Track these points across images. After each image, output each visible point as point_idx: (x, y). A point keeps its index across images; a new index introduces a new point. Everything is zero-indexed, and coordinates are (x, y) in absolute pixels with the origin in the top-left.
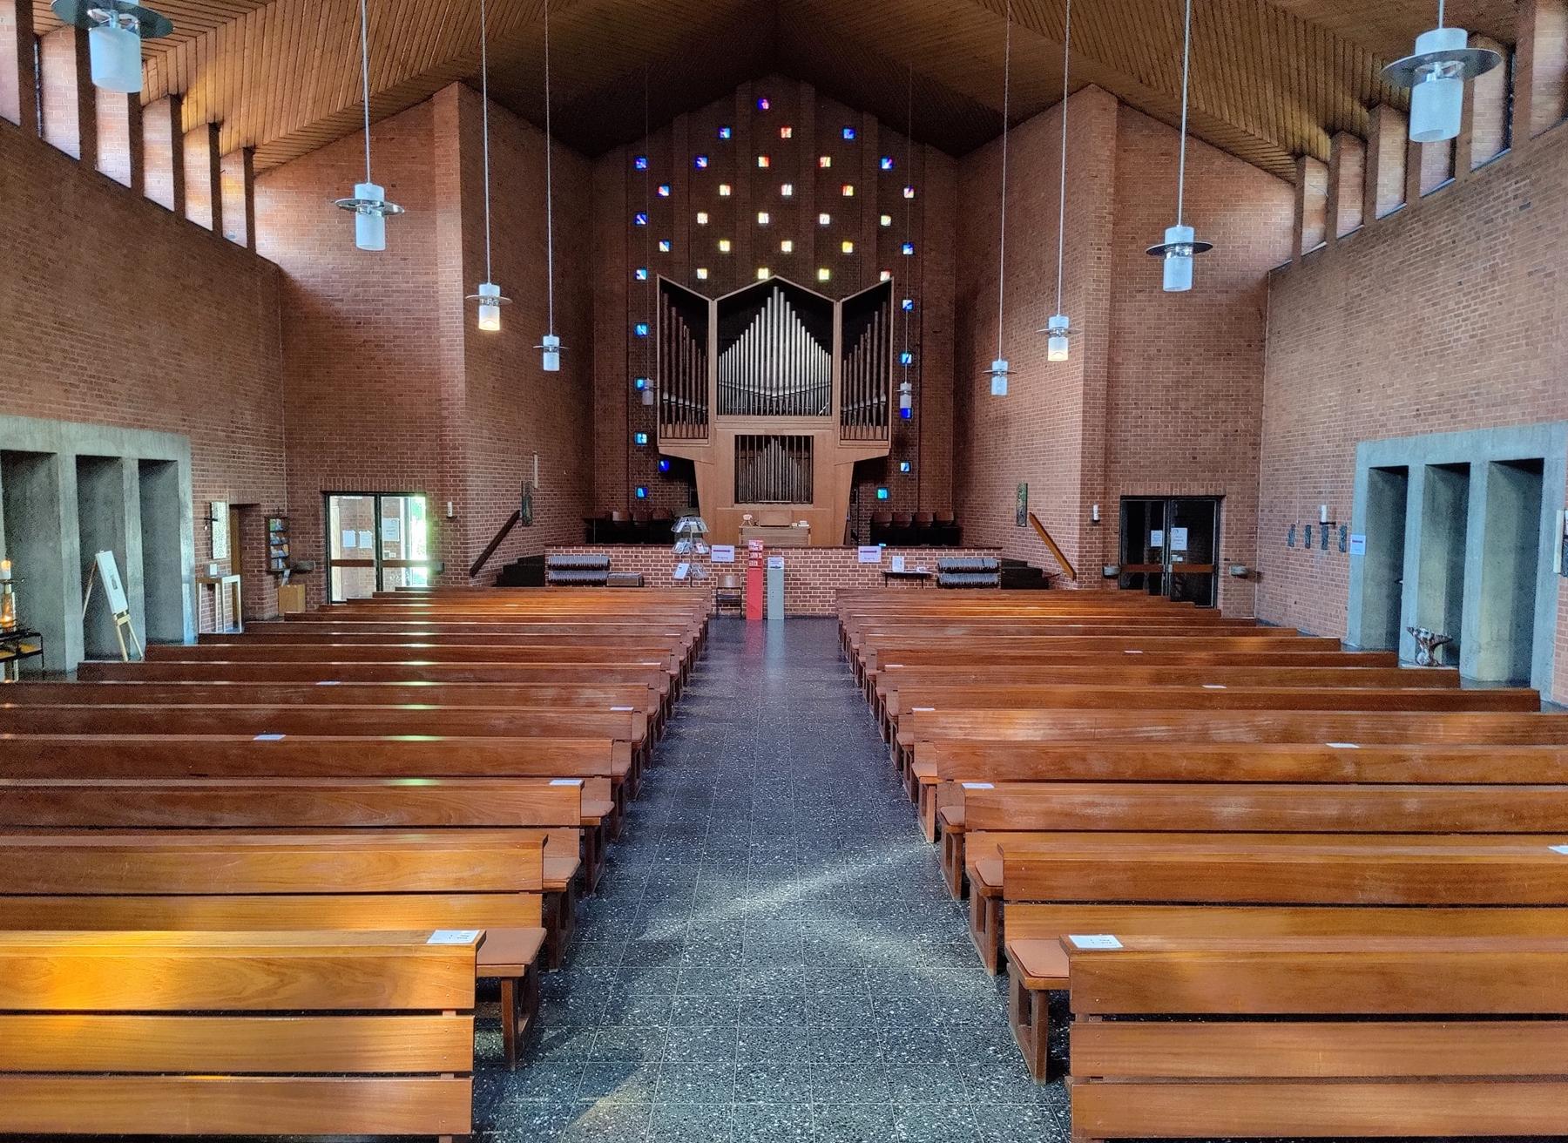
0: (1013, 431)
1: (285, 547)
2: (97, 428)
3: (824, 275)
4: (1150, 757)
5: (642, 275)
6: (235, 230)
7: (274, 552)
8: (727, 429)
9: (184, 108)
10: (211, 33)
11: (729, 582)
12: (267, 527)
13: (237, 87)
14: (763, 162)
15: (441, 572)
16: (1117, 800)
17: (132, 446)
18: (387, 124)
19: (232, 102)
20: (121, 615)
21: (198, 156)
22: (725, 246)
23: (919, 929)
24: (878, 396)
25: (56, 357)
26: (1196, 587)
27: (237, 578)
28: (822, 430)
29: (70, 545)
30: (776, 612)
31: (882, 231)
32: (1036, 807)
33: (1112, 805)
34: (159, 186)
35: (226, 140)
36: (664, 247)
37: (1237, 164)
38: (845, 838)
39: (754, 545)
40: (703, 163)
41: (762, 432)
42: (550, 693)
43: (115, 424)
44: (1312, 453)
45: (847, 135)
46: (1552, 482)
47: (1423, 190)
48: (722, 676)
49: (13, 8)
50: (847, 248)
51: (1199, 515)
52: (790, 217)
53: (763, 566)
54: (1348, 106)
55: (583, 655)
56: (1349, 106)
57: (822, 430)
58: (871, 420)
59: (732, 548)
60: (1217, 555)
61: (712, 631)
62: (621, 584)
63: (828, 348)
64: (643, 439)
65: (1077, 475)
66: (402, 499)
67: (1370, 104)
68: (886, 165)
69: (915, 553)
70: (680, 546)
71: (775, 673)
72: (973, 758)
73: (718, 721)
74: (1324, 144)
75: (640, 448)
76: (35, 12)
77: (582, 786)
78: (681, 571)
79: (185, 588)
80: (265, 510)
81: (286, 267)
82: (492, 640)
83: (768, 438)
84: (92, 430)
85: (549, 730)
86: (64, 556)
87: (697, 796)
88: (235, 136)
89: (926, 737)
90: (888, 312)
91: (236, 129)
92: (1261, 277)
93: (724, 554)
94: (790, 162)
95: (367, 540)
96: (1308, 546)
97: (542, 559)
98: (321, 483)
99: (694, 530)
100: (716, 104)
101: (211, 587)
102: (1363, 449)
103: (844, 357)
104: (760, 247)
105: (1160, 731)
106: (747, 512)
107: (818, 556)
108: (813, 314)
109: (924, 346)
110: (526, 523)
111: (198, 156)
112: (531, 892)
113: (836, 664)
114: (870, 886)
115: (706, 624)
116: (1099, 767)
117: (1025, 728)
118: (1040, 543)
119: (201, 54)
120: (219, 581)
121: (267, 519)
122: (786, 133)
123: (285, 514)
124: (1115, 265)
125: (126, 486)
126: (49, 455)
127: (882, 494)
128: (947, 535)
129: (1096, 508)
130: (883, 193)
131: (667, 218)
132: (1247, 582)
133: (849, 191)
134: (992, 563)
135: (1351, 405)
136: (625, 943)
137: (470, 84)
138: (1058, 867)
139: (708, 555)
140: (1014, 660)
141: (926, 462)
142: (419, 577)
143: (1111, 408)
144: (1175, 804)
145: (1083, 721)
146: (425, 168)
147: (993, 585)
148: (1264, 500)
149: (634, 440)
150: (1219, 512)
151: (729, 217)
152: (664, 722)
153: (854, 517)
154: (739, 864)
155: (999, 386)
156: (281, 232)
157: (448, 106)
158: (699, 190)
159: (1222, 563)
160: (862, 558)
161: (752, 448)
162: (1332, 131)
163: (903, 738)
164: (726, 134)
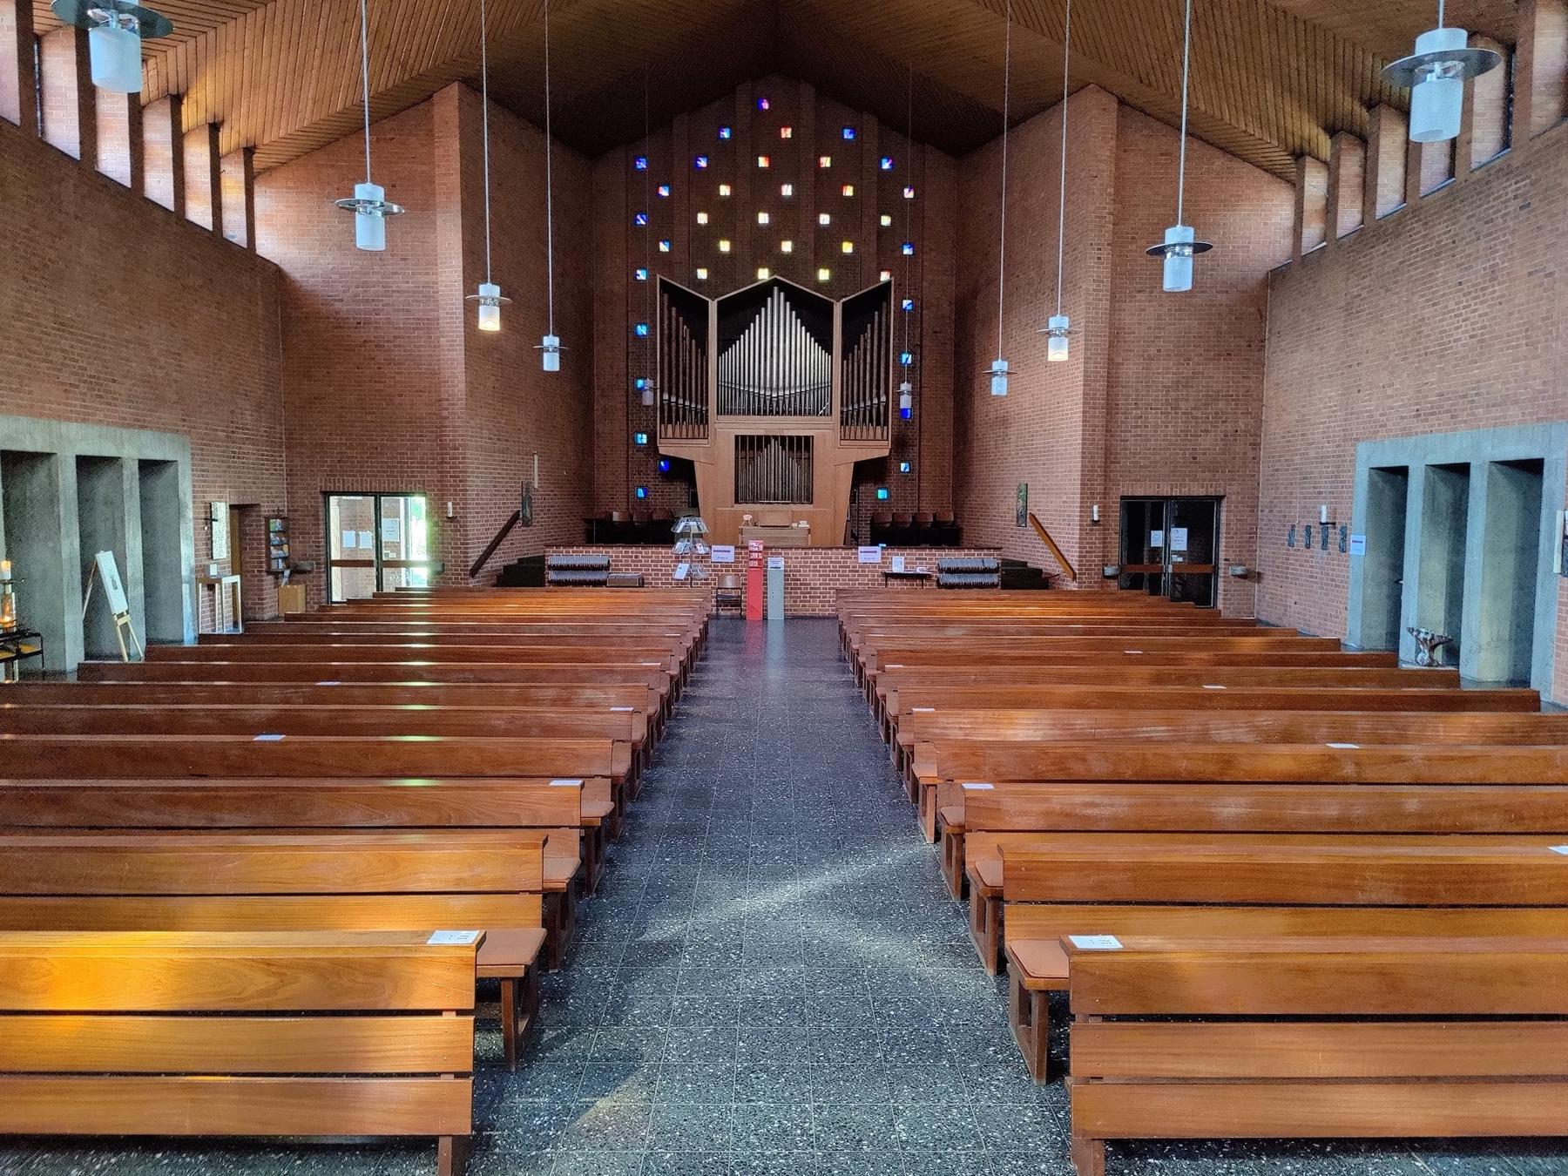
0: (1012, 431)
1: (285, 547)
5: (642, 275)
6: (235, 230)
7: (274, 552)
8: (727, 429)
9: (184, 108)
10: (211, 33)
11: (729, 582)
13: (237, 87)
14: (763, 162)
15: (441, 573)
17: (132, 447)
18: (387, 124)
19: (232, 102)
21: (198, 156)
22: (725, 246)
23: (919, 930)
24: (879, 397)
25: (56, 357)
26: (1196, 588)
27: (237, 579)
28: (822, 430)
29: (70, 545)
30: (776, 613)
31: (882, 231)
33: (1112, 805)
34: (159, 187)
35: (227, 140)
36: (664, 247)
37: (1237, 164)
38: (845, 839)
40: (703, 163)
41: (762, 433)
42: (550, 693)
43: (114, 424)
44: (1312, 454)
45: (847, 135)
46: (1552, 482)
47: (1423, 190)
48: (722, 676)
49: (13, 8)
50: (847, 248)
51: (1199, 515)
53: (763, 566)
54: (1348, 106)
55: (584, 655)
56: (1349, 106)
57: (822, 430)
59: (732, 548)
61: (712, 632)
62: (621, 584)
63: (828, 348)
64: (643, 439)
65: (1077, 476)
66: (402, 499)
67: (1370, 105)
68: (886, 165)
70: (680, 546)
71: (775, 674)
72: (973, 758)
74: (1324, 145)
75: (640, 448)
76: (35, 12)
77: (582, 786)
78: (681, 571)
79: (185, 588)
80: (266, 510)
81: (286, 267)
83: (768, 438)
84: (91, 431)
85: (549, 731)
86: (64, 556)
87: (696, 796)
88: (235, 136)
89: (926, 737)
90: (888, 313)
91: (236, 129)
92: (1261, 276)
93: (724, 554)
94: (790, 162)
96: (1308, 546)
97: (542, 559)
98: (321, 483)
99: (695, 530)
100: (716, 104)
101: (211, 587)
102: (1363, 449)
103: (844, 357)
104: (760, 247)
106: (747, 512)
107: (818, 556)
108: (813, 315)
109: (924, 345)
110: (527, 523)
111: (198, 156)
113: (836, 664)
114: (871, 886)
115: (706, 625)
116: (1099, 767)
117: (1026, 728)
118: (1041, 544)
120: (219, 581)
121: (267, 519)
123: (285, 514)
124: (1114, 265)
125: (126, 486)
126: (49, 455)
127: (882, 494)
128: (947, 535)
129: (1095, 508)
130: (883, 193)
131: (667, 219)
132: (1247, 582)
133: (849, 191)
134: (992, 563)
135: (1351, 406)
137: (471, 84)
138: (1057, 867)
139: (708, 555)
140: (1014, 660)
141: (926, 462)
142: (419, 577)
143: (1111, 408)
144: (1175, 804)
145: (1082, 721)
146: (425, 168)
147: (993, 586)
148: (1263, 500)
149: (634, 440)
150: (1219, 512)
151: (729, 217)
152: (664, 722)
153: (854, 516)
154: (739, 864)
155: (999, 387)
156: (281, 232)
157: (448, 106)
158: (699, 190)
159: (1222, 564)
160: (862, 558)
161: (752, 448)
162: (1332, 131)
163: (903, 738)
164: (726, 134)
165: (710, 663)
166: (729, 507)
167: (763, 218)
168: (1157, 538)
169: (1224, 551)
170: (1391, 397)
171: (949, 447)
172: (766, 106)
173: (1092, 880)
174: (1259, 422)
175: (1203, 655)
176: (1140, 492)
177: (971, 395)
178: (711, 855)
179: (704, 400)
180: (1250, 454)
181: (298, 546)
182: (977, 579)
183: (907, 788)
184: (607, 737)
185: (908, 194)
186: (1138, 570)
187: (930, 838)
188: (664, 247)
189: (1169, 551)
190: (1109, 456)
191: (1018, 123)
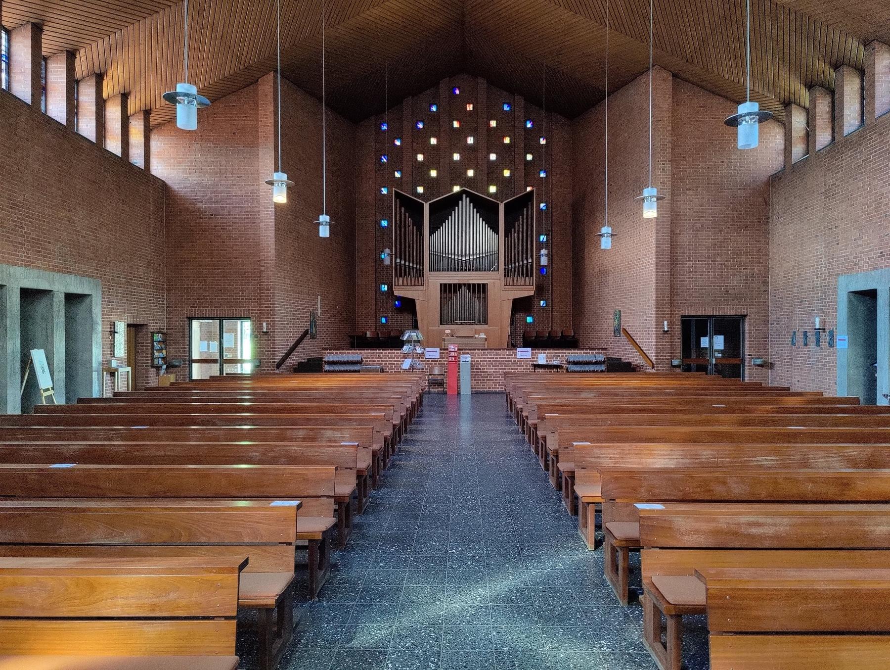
1: (164, 351)
2: (36, 271)
3: (493, 189)
4: (781, 481)
5: (384, 191)
6: (137, 157)
7: (156, 354)
8: (435, 280)
9: (105, 83)
10: (119, 33)
11: (436, 371)
12: (152, 337)
13: (137, 73)
14: (456, 124)
15: (259, 364)
16: (779, 520)
17: (61, 285)
20: (48, 390)
21: (113, 113)
23: (598, 637)
24: (527, 259)
27: (129, 369)
28: (493, 280)
31: (527, 163)
32: (704, 526)
33: (775, 525)
34: (87, 127)
35: (133, 105)
36: (397, 175)
38: (520, 547)
39: (452, 347)
40: (420, 126)
41: (456, 282)
42: (301, 433)
43: (48, 269)
44: (806, 285)
45: (506, 108)
47: (877, 114)
48: (431, 430)
50: (507, 173)
51: (731, 327)
52: (471, 156)
53: (457, 361)
54: (821, 69)
55: (335, 410)
56: (821, 68)
57: (493, 280)
58: (523, 274)
59: (438, 350)
60: (743, 353)
61: (426, 401)
62: (368, 371)
63: (496, 231)
64: (385, 288)
65: (653, 303)
66: (239, 322)
68: (529, 125)
69: (552, 352)
70: (406, 348)
71: (465, 427)
72: (630, 485)
73: (426, 456)
74: (805, 97)
75: (384, 293)
76: (3, 14)
77: (299, 507)
78: (407, 364)
79: (95, 375)
81: (169, 183)
82: (273, 400)
83: (460, 285)
84: (33, 273)
85: (293, 460)
86: (9, 351)
87: (410, 511)
88: (138, 102)
89: (584, 464)
90: (532, 209)
91: (138, 97)
92: (765, 179)
93: (433, 353)
94: (472, 124)
95: (214, 346)
96: (806, 345)
97: (321, 359)
98: (187, 312)
99: (415, 338)
100: (428, 92)
101: (112, 374)
102: (842, 280)
103: (506, 236)
105: (769, 460)
106: (447, 330)
107: (489, 354)
108: (486, 210)
109: (556, 228)
110: (313, 337)
111: (113, 113)
112: (227, 618)
113: (505, 420)
114: (548, 588)
115: (421, 395)
116: (737, 489)
117: (660, 458)
118: (630, 346)
119: (114, 52)
120: (117, 370)
121: (153, 333)
122: (470, 107)
123: (165, 331)
124: (673, 174)
125: (55, 308)
128: (570, 343)
129: (666, 323)
130: (528, 141)
131: (398, 158)
132: (764, 370)
133: (507, 140)
134: (601, 358)
136: (335, 650)
138: (763, 596)
139: (423, 354)
140: (634, 411)
141: (556, 300)
142: (247, 369)
144: (831, 524)
145: (706, 452)
146: (252, 123)
147: (602, 371)
148: (772, 318)
149: (380, 288)
150: (743, 324)
151: (436, 157)
152: (386, 459)
153: (513, 334)
154: (440, 569)
155: (606, 243)
156: (167, 164)
158: (419, 141)
159: (747, 357)
161: (450, 291)
163: (564, 466)
164: (434, 109)
165: (424, 419)
166: (437, 327)
167: (456, 157)
168: (705, 342)
169: (748, 349)
170: (860, 246)
171: (570, 291)
172: (457, 92)
173: (800, 609)
174: (767, 269)
175: (769, 407)
176: (693, 313)
177: (583, 259)
178: (417, 560)
179: (421, 262)
180: (763, 288)
181: (172, 349)
182: (592, 368)
183: (566, 504)
184: (332, 464)
185: (543, 142)
186: (691, 359)
187: (591, 546)
188: (397, 175)
189: (712, 346)
190: (673, 291)
191: (613, 92)
